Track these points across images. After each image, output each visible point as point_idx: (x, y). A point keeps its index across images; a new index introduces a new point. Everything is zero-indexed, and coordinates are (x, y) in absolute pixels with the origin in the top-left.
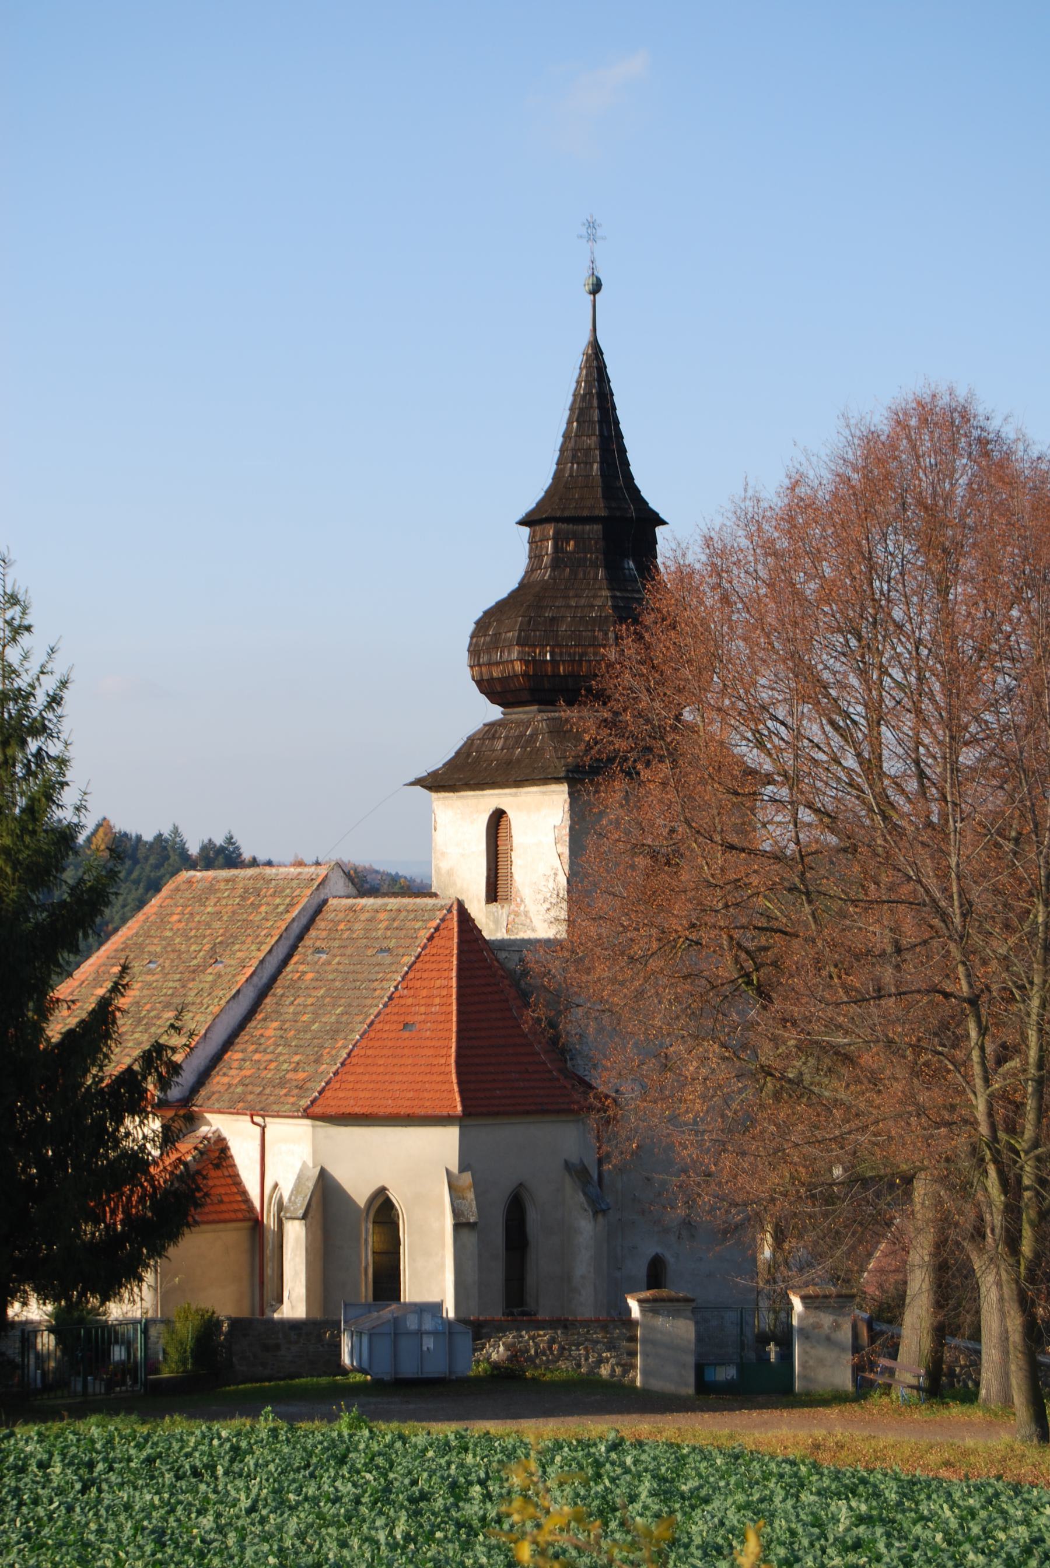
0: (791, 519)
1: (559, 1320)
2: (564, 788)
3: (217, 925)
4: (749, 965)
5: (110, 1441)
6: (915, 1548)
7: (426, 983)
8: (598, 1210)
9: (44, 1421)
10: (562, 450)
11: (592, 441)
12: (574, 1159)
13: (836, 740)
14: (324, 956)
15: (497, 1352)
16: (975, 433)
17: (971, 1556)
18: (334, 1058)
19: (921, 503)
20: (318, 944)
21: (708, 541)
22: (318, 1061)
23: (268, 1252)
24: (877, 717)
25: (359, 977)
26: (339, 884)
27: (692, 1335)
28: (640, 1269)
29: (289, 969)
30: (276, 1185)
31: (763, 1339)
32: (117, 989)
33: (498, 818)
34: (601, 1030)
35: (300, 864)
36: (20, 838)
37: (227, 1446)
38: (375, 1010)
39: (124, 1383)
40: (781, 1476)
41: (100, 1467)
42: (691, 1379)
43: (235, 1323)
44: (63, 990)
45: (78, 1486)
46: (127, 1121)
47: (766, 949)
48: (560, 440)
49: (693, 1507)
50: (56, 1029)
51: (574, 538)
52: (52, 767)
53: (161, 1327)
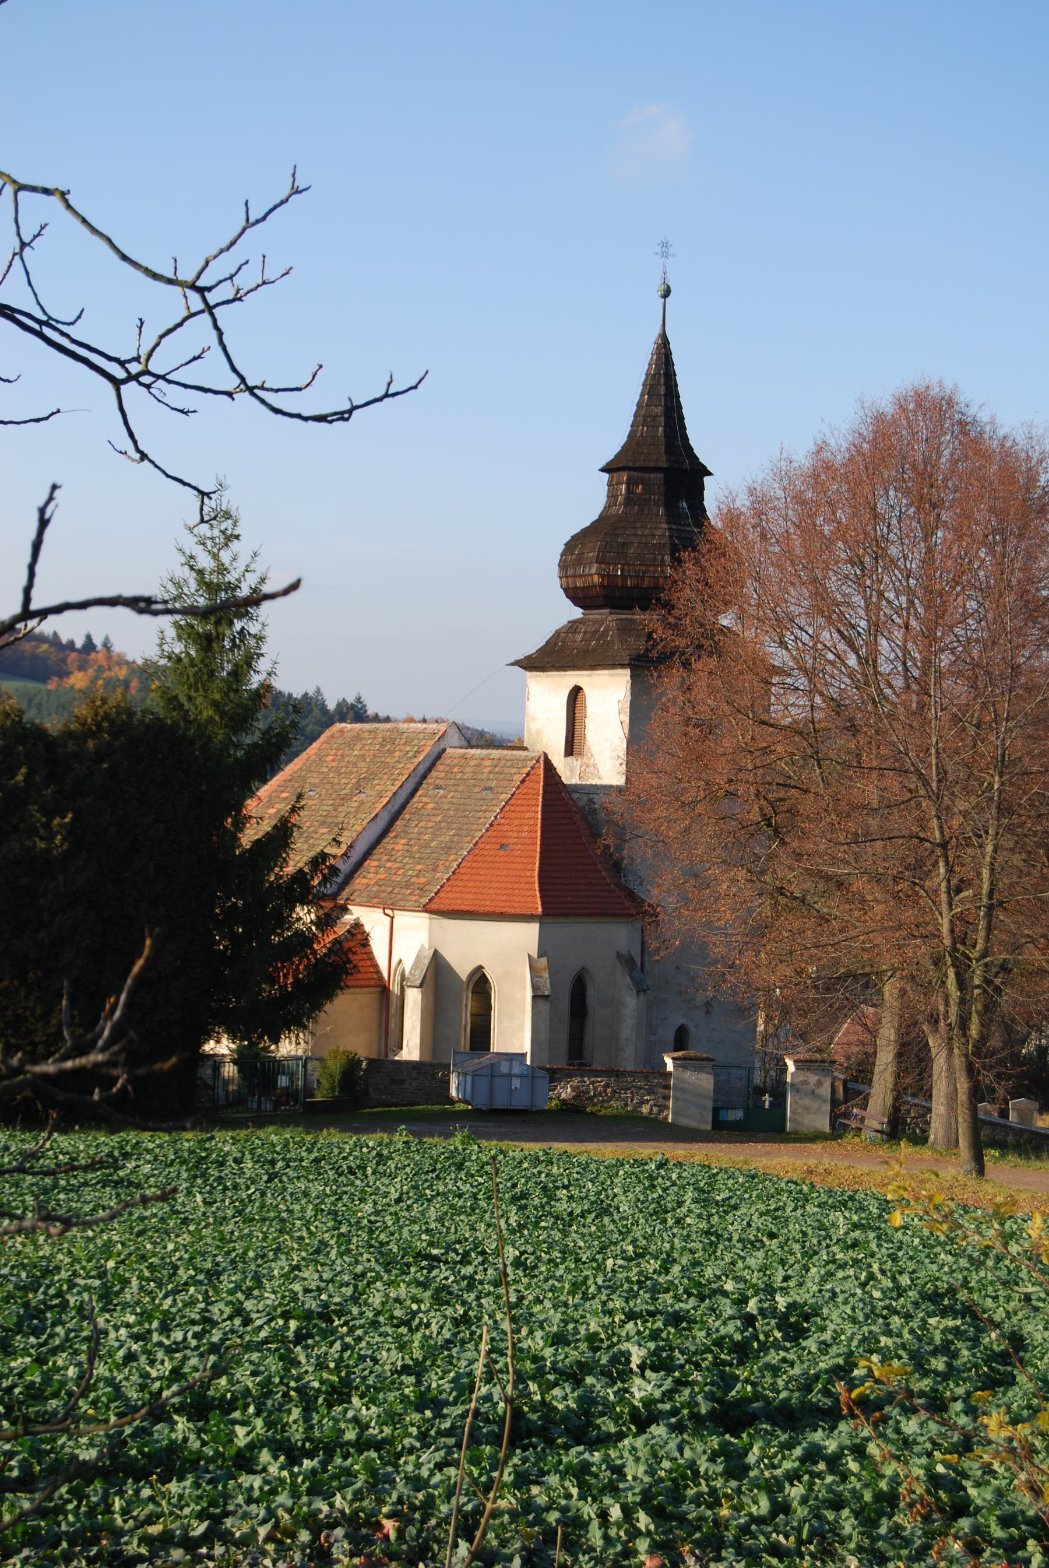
0: (816, 476)
1: (612, 1071)
2: (627, 672)
3: (362, 764)
4: (769, 811)
5: (286, 1145)
6: (900, 1249)
7: (518, 815)
8: (641, 989)
9: (234, 1129)
10: (636, 416)
11: (659, 410)
12: (624, 951)
13: (842, 646)
14: (442, 792)
15: (566, 1092)
16: (957, 417)
17: (943, 1256)
18: (447, 868)
19: (914, 467)
20: (438, 782)
21: (751, 492)
22: (435, 870)
23: (392, 1011)
24: (876, 628)
25: (469, 808)
26: (454, 738)
27: (711, 1087)
28: (670, 1035)
29: (415, 800)
30: (400, 961)
31: (760, 1091)
32: (294, 810)
33: (576, 693)
34: (656, 855)
35: (411, 720)
36: (226, 694)
37: (374, 1153)
38: (479, 834)
39: (288, 1104)
40: (791, 1192)
41: (280, 1164)
42: (710, 1119)
43: (371, 1062)
44: (251, 806)
45: (265, 1178)
46: (298, 909)
47: (782, 800)
48: (635, 408)
49: (726, 1212)
50: (249, 836)
51: (642, 483)
52: (252, 642)
53: (317, 1063)
